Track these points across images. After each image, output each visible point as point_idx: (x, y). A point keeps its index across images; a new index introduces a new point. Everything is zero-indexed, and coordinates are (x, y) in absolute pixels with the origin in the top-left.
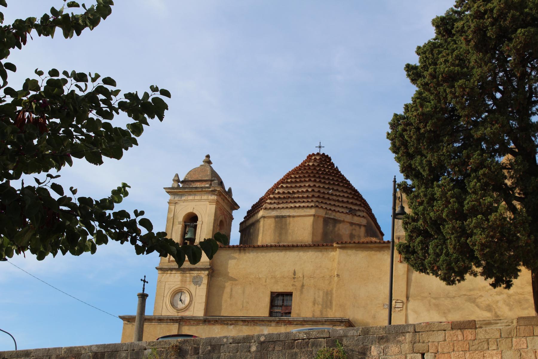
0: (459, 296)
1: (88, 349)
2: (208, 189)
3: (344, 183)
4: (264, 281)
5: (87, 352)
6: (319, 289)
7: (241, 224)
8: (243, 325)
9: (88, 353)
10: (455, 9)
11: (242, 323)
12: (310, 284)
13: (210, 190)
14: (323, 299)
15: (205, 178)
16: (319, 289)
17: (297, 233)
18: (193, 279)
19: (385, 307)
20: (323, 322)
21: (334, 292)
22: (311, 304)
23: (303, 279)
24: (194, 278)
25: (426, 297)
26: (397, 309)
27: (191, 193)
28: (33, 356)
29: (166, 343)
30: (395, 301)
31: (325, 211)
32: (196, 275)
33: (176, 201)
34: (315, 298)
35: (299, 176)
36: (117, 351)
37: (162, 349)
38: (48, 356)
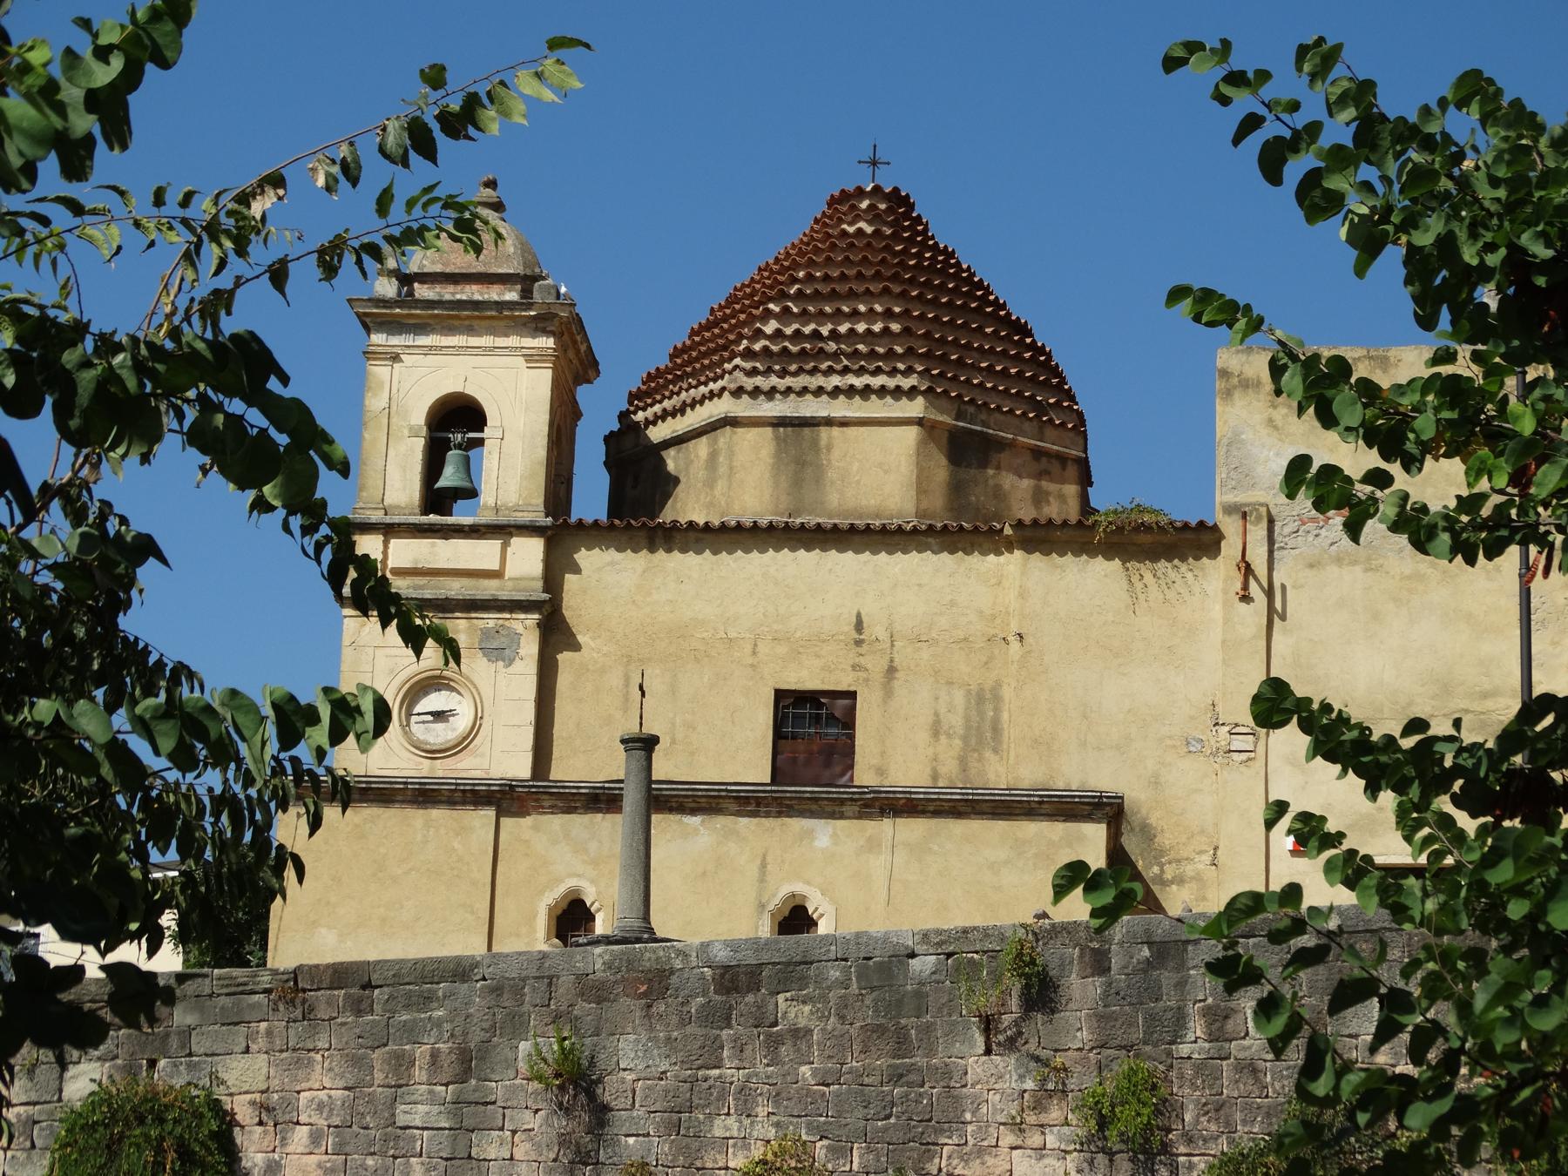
0: (1444, 715)
1: (694, 954)
2: (525, 310)
3: (904, 281)
4: (748, 648)
5: (694, 964)
6: (952, 683)
7: (609, 439)
8: (739, 814)
9: (699, 967)
11: (734, 807)
12: (917, 666)
13: (532, 313)
14: (967, 719)
15: (500, 266)
16: (952, 683)
17: (858, 482)
18: (481, 641)
19: (1192, 749)
20: (1033, 805)
21: (1007, 693)
22: (923, 736)
23: (893, 646)
24: (486, 634)
26: (1235, 755)
27: (456, 323)
28: (484, 979)
29: (987, 935)
30: (1227, 729)
31: (956, 406)
32: (491, 624)
33: (395, 350)
34: (936, 714)
35: (842, 273)
36: (806, 963)
37: (975, 956)
38: (543, 977)
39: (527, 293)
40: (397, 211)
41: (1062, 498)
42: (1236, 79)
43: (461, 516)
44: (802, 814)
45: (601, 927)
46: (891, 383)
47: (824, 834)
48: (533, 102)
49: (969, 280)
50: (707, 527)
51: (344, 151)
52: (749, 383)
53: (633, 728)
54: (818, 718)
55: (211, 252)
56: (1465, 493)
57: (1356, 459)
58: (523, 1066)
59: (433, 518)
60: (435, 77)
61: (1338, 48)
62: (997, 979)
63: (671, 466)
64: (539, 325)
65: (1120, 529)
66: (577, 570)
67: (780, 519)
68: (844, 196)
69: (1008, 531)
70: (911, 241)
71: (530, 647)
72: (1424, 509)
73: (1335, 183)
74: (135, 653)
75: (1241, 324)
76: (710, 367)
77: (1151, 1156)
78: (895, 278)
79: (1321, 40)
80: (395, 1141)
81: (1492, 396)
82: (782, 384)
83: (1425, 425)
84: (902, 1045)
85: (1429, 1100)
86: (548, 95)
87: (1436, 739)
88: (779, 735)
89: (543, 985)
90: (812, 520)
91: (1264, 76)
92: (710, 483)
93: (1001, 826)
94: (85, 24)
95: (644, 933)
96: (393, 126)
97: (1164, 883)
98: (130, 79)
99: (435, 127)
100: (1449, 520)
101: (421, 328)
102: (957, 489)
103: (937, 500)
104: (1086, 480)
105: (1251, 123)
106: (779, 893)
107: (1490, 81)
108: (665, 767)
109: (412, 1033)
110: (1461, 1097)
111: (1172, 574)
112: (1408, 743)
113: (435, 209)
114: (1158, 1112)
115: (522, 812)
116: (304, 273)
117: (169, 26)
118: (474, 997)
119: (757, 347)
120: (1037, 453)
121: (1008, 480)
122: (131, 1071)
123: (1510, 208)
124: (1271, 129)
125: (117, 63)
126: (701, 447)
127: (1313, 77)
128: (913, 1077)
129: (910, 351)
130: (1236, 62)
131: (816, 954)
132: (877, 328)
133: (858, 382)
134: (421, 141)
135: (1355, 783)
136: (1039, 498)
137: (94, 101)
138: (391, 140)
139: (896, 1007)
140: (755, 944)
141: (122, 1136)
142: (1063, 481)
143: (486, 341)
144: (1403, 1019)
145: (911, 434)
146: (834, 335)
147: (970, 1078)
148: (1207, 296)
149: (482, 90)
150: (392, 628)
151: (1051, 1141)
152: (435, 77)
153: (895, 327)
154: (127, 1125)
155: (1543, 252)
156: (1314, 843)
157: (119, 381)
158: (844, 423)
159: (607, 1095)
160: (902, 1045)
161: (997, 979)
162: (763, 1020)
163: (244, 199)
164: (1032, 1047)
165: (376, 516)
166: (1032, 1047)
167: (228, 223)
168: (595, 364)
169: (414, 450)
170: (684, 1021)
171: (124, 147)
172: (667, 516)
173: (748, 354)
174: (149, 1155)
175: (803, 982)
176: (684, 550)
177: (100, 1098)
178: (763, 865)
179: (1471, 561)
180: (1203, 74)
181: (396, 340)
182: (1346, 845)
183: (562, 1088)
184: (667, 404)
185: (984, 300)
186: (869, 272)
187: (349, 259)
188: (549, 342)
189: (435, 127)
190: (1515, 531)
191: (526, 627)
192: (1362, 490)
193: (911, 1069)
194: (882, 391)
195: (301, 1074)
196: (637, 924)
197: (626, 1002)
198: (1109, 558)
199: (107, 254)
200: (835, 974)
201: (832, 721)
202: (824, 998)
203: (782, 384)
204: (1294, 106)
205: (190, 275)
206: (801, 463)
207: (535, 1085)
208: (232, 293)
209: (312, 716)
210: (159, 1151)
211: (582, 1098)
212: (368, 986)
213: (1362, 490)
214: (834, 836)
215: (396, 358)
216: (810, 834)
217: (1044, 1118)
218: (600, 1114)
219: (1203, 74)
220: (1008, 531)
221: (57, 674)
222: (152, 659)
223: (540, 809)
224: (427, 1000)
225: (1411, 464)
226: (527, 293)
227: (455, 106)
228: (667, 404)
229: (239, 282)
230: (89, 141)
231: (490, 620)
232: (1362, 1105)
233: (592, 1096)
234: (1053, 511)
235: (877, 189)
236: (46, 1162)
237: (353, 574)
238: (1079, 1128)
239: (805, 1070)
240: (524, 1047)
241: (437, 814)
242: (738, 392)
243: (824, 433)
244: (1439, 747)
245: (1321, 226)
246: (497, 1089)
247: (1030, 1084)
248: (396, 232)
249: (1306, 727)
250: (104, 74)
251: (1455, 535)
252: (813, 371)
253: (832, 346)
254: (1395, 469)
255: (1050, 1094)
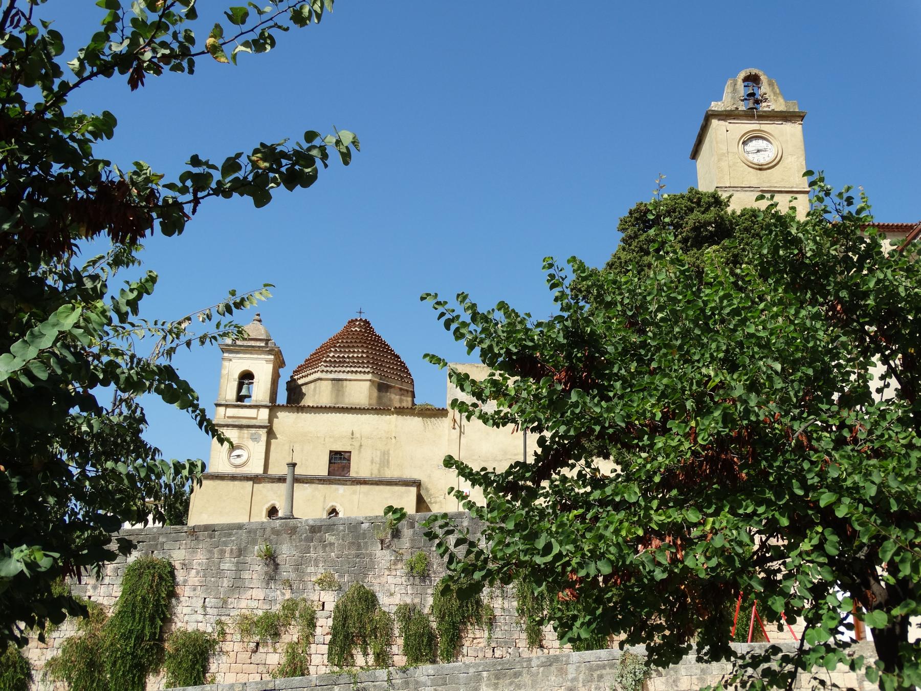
8: (319, 484)
10: (187, 70)
14: (380, 459)
21: (391, 452)
22: (369, 463)
24: (252, 434)
25: (476, 460)
39: (267, 344)
40: (222, 328)
41: (407, 401)
42: (439, 303)
43: (247, 402)
44: (335, 484)
45: (280, 514)
46: (363, 370)
47: (341, 489)
48: (259, 300)
49: (384, 344)
50: (313, 407)
51: (207, 312)
52: (325, 369)
53: (290, 461)
54: (341, 458)
55: (169, 338)
56: (497, 410)
57: (469, 399)
58: (256, 553)
59: (239, 403)
60: (233, 293)
61: (467, 295)
62: (385, 530)
63: (304, 391)
64: (270, 352)
65: (422, 410)
66: (277, 417)
67: (332, 405)
68: (352, 321)
69: (392, 409)
70: (369, 333)
71: (264, 438)
72: (486, 414)
73: (463, 331)
74: (143, 445)
75: (441, 364)
76: (316, 364)
77: (424, 577)
78: (365, 343)
79: (463, 293)
80: (220, 573)
81: (504, 385)
82: (334, 369)
83: (487, 392)
84: (359, 547)
85: (480, 570)
86: (263, 299)
87: (489, 473)
88: (330, 463)
89: (262, 531)
90: (341, 406)
91: (446, 303)
92: (314, 395)
93: (388, 488)
94: (128, 282)
95: (291, 517)
96: (221, 306)
97: (431, 503)
98: (139, 297)
99: (232, 306)
100: (493, 417)
101: (238, 352)
102: (379, 398)
103: (374, 401)
104: (413, 396)
105: (442, 314)
106: (328, 507)
107: (507, 304)
108: (298, 471)
109: (226, 544)
110: (488, 570)
111: (435, 422)
112: (482, 473)
113: (232, 327)
114: (427, 565)
115: (260, 483)
116: (196, 343)
117: (151, 284)
118: (243, 534)
119: (328, 360)
120: (401, 389)
121: (393, 396)
122: (146, 554)
123: (507, 338)
124: (447, 316)
125: (136, 293)
126: (312, 386)
127: (461, 302)
128: (362, 556)
129: (368, 362)
130: (439, 299)
131: (337, 523)
132: (360, 355)
133: (354, 370)
134: (229, 309)
135: (469, 483)
136: (401, 401)
137: (128, 303)
138: (220, 310)
139: (357, 537)
140: (321, 520)
141: (143, 572)
142: (407, 397)
143: (255, 356)
144: (473, 550)
145: (368, 383)
146: (348, 357)
147: (377, 556)
148: (433, 356)
149: (245, 297)
150: (215, 438)
151: (398, 573)
152: (233, 293)
153: (364, 355)
154: (145, 569)
155: (515, 350)
156: (460, 498)
157: (132, 377)
158: (350, 380)
159: (278, 561)
160: (359, 547)
161: (385, 530)
162: (322, 541)
163: (180, 323)
164: (394, 548)
165: (223, 402)
166: (394, 548)
167: (175, 330)
168: (284, 363)
169: (235, 385)
170: (301, 541)
171: (137, 315)
172: (302, 404)
173: (325, 361)
174: (150, 578)
175: (333, 530)
176: (306, 413)
177: (138, 562)
178: (325, 497)
179: (498, 427)
180: (430, 302)
181: (231, 355)
182: (469, 499)
183: (266, 559)
184: (303, 374)
185: (388, 349)
186: (358, 341)
187: (208, 340)
188: (272, 357)
189: (232, 306)
190: (509, 420)
191: (263, 433)
192: (471, 408)
193: (361, 554)
194: (361, 372)
195: (194, 555)
196: (289, 514)
197: (285, 536)
198: (419, 417)
199: (141, 337)
200: (341, 528)
201: (345, 458)
202: (338, 535)
203: (334, 369)
204: (453, 311)
205: (164, 343)
206: (338, 390)
207: (259, 558)
208: (175, 348)
209: (184, 467)
210: (153, 576)
211: (272, 562)
212: (214, 531)
213: (471, 408)
214: (344, 491)
215: (230, 360)
216: (337, 489)
217: (396, 567)
218: (277, 566)
219: (430, 302)
220: (392, 409)
221: (121, 450)
222: (148, 447)
223: (265, 482)
224: (230, 535)
225: (484, 401)
226: (267, 344)
227: (238, 301)
228: (303, 374)
229: (177, 345)
230: (127, 313)
231: (253, 431)
232: (463, 572)
233: (274, 561)
234: (405, 405)
235: (361, 319)
236: (121, 580)
237: (205, 424)
238: (406, 570)
239: (333, 554)
240: (256, 548)
241: (237, 483)
242: (323, 371)
243: (345, 382)
244: (489, 475)
245: (459, 341)
246: (249, 559)
247: (393, 558)
248: (221, 333)
249: (457, 468)
250: (132, 296)
251: (494, 421)
252: (343, 366)
253: (348, 360)
254: (480, 403)
255: (398, 561)
